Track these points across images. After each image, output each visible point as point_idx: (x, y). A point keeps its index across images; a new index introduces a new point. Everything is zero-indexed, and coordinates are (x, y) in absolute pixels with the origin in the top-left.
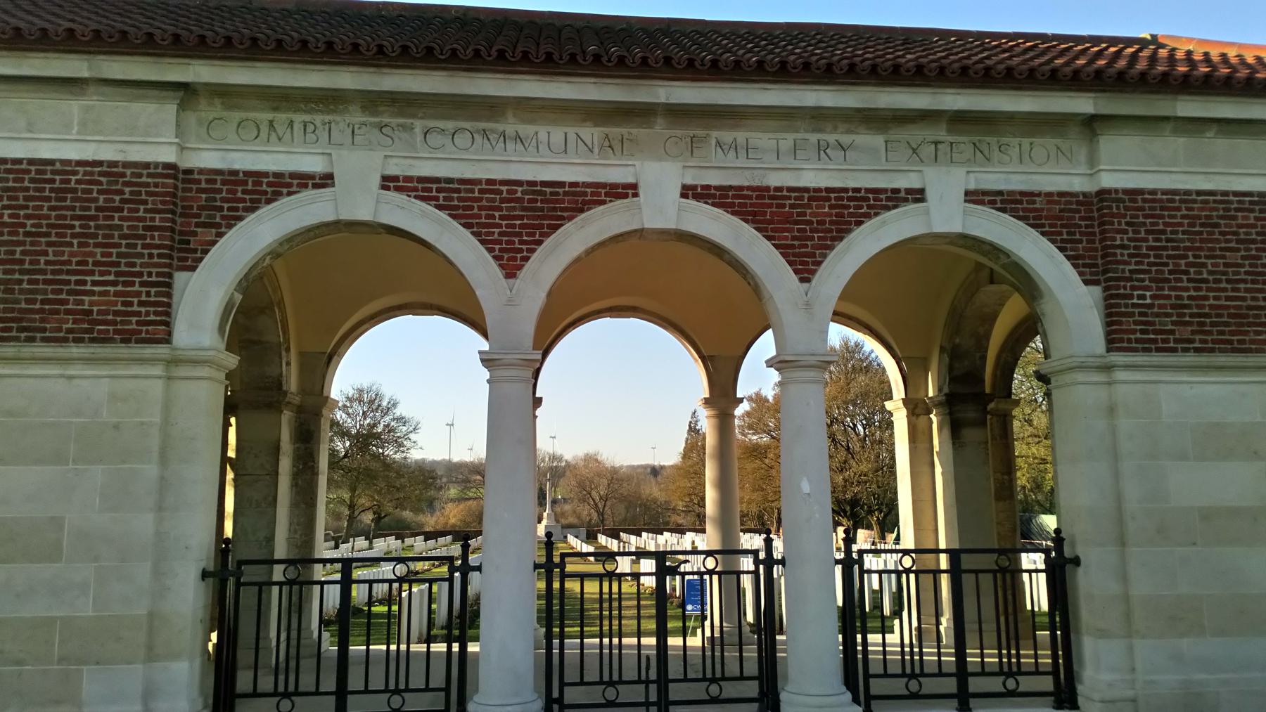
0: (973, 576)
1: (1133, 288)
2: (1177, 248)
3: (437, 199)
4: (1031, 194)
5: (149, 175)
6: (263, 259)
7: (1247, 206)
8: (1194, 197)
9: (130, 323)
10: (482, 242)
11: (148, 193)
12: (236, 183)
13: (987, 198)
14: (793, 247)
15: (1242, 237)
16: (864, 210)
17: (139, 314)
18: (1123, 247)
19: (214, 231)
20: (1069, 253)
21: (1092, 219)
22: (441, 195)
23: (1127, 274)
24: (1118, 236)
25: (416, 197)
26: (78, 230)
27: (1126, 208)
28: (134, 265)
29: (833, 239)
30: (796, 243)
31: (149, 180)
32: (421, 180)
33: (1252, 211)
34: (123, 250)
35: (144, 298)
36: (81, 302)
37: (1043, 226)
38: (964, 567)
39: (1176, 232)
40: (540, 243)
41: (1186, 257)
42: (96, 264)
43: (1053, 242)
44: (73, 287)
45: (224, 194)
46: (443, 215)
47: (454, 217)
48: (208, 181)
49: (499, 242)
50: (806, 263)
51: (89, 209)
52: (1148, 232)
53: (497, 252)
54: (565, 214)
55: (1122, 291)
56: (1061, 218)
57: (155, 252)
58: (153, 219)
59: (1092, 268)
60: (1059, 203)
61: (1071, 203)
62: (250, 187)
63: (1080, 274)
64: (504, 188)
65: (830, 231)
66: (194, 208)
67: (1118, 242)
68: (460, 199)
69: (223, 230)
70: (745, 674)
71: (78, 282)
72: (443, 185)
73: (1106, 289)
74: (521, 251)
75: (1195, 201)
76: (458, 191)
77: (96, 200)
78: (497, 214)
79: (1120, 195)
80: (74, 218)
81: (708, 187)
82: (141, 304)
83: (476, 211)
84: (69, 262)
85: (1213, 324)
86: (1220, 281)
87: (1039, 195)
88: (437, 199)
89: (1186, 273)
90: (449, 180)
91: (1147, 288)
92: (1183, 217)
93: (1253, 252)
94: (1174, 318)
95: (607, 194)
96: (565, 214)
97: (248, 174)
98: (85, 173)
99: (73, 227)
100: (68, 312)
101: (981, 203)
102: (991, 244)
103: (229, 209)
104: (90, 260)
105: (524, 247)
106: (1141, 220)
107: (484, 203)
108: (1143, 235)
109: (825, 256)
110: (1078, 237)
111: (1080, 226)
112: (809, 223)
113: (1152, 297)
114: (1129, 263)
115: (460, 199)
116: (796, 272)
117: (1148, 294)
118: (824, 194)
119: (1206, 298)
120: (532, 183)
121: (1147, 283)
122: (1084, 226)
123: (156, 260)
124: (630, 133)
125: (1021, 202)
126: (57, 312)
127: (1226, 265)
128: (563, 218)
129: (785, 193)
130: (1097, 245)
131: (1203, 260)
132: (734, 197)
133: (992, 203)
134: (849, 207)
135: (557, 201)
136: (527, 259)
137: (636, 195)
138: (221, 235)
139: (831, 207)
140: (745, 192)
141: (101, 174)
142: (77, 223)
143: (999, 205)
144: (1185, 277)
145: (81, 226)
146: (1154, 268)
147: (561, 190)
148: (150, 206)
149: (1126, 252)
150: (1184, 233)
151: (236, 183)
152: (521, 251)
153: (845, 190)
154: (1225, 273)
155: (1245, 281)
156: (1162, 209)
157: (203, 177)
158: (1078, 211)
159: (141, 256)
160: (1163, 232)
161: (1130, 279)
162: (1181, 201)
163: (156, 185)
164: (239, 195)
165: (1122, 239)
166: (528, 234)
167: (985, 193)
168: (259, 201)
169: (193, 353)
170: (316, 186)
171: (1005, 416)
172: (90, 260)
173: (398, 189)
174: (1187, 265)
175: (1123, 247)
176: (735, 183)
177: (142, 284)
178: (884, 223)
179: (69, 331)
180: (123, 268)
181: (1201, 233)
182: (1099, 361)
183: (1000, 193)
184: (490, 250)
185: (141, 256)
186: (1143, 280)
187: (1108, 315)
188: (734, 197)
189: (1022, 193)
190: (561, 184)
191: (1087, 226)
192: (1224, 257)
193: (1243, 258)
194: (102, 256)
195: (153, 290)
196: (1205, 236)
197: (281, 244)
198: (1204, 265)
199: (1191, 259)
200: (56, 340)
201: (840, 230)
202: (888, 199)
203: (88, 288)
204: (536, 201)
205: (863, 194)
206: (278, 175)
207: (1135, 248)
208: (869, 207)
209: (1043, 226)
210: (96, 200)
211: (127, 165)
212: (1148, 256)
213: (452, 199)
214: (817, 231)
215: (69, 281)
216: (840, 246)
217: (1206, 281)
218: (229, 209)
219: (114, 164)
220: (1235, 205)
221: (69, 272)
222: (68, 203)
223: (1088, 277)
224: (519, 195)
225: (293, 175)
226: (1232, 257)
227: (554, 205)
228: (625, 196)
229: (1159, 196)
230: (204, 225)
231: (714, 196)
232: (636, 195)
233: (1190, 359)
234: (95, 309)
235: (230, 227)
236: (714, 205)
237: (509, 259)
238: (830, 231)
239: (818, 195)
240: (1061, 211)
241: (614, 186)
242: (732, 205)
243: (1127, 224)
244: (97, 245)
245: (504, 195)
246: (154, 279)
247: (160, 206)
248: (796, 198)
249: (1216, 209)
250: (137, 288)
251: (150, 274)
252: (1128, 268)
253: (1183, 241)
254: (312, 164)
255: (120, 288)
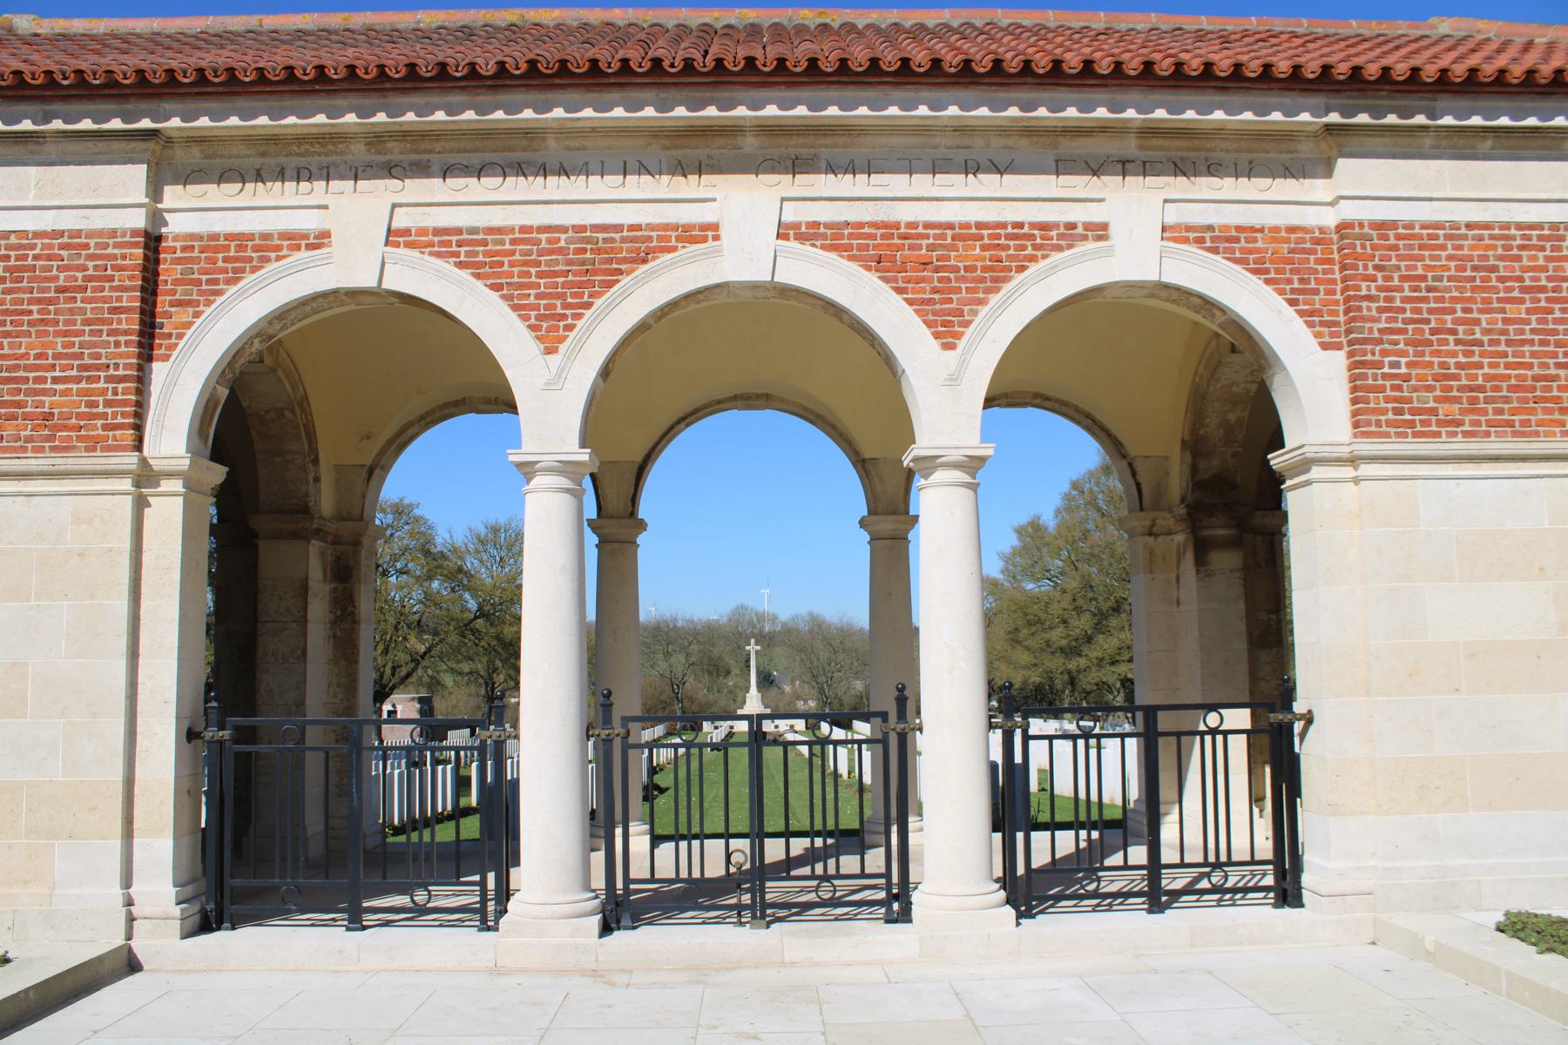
0: (1173, 739)
1: (1384, 353)
2: (1442, 300)
3: (457, 254)
4: (1252, 229)
5: (116, 246)
6: (250, 341)
7: (1534, 242)
8: (1463, 231)
9: (95, 427)
10: (515, 308)
11: (114, 268)
12: (217, 249)
13: (1192, 235)
14: (931, 301)
15: (1528, 283)
16: (1029, 251)
17: (104, 416)
18: (1369, 298)
19: (191, 310)
20: (1302, 307)
21: (1330, 261)
22: (463, 250)
23: (1376, 335)
24: (1364, 285)
25: (432, 254)
26: (36, 316)
27: (1374, 248)
28: (98, 356)
29: (988, 291)
30: (937, 296)
31: (116, 251)
32: (438, 232)
33: (1542, 249)
34: (87, 338)
35: (110, 396)
36: (41, 404)
37: (1267, 271)
38: (1161, 727)
39: (1440, 279)
40: (588, 306)
41: (1453, 311)
42: (57, 356)
43: (1281, 292)
44: (31, 385)
45: (202, 264)
46: (465, 275)
47: (478, 276)
48: (184, 249)
49: (536, 307)
50: (951, 323)
51: (48, 290)
52: (1403, 278)
53: (533, 321)
54: (623, 267)
55: (1369, 357)
56: (1290, 261)
57: (122, 339)
58: (119, 299)
59: (1336, 326)
60: (1288, 241)
61: (1303, 241)
62: (232, 254)
63: (1317, 335)
64: (543, 237)
65: (983, 280)
66: (153, 283)
67: (1364, 293)
68: (486, 254)
69: (201, 308)
70: (867, 871)
71: (37, 380)
72: (465, 236)
73: (1351, 354)
74: (564, 317)
75: (1465, 237)
76: (484, 243)
77: (56, 278)
78: (533, 270)
79: (1366, 230)
80: (30, 302)
81: (816, 224)
82: (108, 404)
83: (506, 268)
84: (25, 356)
85: (1487, 400)
86: (1498, 342)
87: (1262, 230)
88: (457, 254)
89: (1453, 332)
90: (473, 230)
91: (1404, 354)
92: (1450, 258)
93: (1543, 304)
94: (1438, 393)
95: (678, 239)
96: (623, 267)
97: (230, 237)
98: (44, 247)
99: (30, 312)
100: (26, 417)
101: (1186, 241)
102: (1200, 296)
103: (209, 282)
104: (50, 352)
105: (568, 312)
106: (1394, 262)
107: (517, 257)
108: (1396, 282)
109: (975, 313)
110: (1313, 285)
111: (1316, 271)
112: (956, 269)
113: (1409, 365)
114: (1378, 320)
115: (486, 254)
116: (937, 336)
117: (1403, 360)
118: (974, 231)
119: (1479, 366)
120: (579, 229)
121: (1401, 346)
122: (1279, 258)
123: (123, 349)
124: (709, 157)
125: (1237, 240)
126: (14, 417)
127: (1505, 321)
128: (620, 272)
129: (921, 230)
130: (1338, 296)
131: (1475, 315)
132: (851, 236)
133: (1200, 241)
134: (1007, 248)
135: (612, 250)
136: (570, 328)
137: (716, 238)
138: (197, 315)
139: (983, 248)
140: (866, 230)
141: (62, 247)
142: (34, 308)
143: (1208, 244)
144: (1451, 338)
145: (39, 312)
146: (1410, 327)
147: (617, 236)
148: (116, 283)
149: (1374, 305)
150: (1450, 279)
151: (217, 249)
152: (564, 317)
153: (1003, 225)
154: (1504, 332)
155: (1531, 343)
156: (1421, 247)
157: (178, 244)
158: (1314, 252)
159: (106, 344)
160: (1423, 278)
161: (1380, 342)
162: (1447, 237)
163: (124, 257)
164: (220, 264)
165: (1369, 288)
166: (574, 295)
167: (1189, 228)
168: (243, 270)
169: (165, 462)
170: (310, 247)
171: (1273, 534)
172: (50, 352)
173: (409, 245)
174: (1454, 321)
175: (1369, 298)
176: (852, 218)
177: (109, 379)
178: (1054, 269)
179: (29, 439)
180: (87, 361)
181: (1473, 279)
182: (1344, 451)
183: (1210, 228)
184: (525, 318)
185: (106, 344)
186: (1396, 343)
187: (1354, 390)
188: (851, 236)
189: (1239, 228)
190: (618, 228)
191: (1325, 272)
192: (1503, 311)
193: (1528, 311)
194: (64, 347)
195: (120, 386)
196: (1478, 283)
197: (270, 323)
198: (1477, 322)
199: (1459, 314)
200: (14, 450)
201: (996, 275)
202: (1060, 236)
203: (48, 386)
204: (584, 251)
205: (1026, 230)
206: (266, 236)
207: (1387, 299)
208: (1035, 247)
209: (1267, 271)
210: (56, 278)
211: (91, 234)
212: (1403, 310)
213: (476, 254)
214: (964, 279)
215: (27, 379)
216: (994, 299)
217: (1479, 343)
218: (209, 282)
219: (77, 234)
220: (1519, 242)
221: (27, 368)
222: (25, 284)
223: (1327, 339)
224: (562, 244)
225: (286, 235)
226: (1512, 311)
227: (606, 257)
228: (704, 240)
229: (1417, 231)
230: (179, 303)
231: (824, 236)
232: (716, 238)
233: (1460, 446)
234: (56, 411)
235: (209, 303)
236: (823, 247)
237: (549, 330)
238: (983, 280)
239: (965, 233)
240: (1291, 251)
241: (687, 228)
242: (848, 248)
243: (1376, 267)
244: (57, 334)
245: (544, 245)
246: (121, 372)
247: (127, 283)
248: (936, 237)
249: (1494, 248)
250: (102, 385)
251: (117, 367)
252: (1376, 326)
253: (1449, 290)
254: (307, 222)
255: (83, 385)
